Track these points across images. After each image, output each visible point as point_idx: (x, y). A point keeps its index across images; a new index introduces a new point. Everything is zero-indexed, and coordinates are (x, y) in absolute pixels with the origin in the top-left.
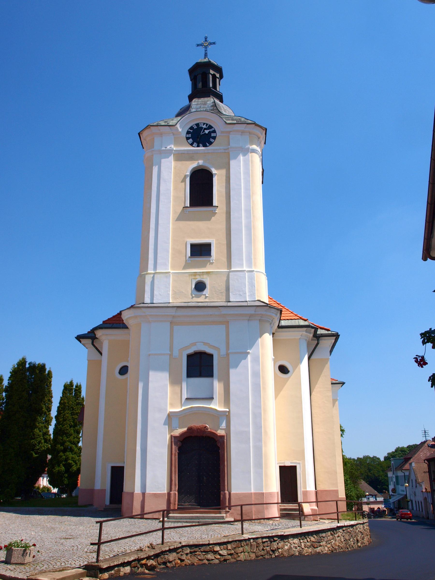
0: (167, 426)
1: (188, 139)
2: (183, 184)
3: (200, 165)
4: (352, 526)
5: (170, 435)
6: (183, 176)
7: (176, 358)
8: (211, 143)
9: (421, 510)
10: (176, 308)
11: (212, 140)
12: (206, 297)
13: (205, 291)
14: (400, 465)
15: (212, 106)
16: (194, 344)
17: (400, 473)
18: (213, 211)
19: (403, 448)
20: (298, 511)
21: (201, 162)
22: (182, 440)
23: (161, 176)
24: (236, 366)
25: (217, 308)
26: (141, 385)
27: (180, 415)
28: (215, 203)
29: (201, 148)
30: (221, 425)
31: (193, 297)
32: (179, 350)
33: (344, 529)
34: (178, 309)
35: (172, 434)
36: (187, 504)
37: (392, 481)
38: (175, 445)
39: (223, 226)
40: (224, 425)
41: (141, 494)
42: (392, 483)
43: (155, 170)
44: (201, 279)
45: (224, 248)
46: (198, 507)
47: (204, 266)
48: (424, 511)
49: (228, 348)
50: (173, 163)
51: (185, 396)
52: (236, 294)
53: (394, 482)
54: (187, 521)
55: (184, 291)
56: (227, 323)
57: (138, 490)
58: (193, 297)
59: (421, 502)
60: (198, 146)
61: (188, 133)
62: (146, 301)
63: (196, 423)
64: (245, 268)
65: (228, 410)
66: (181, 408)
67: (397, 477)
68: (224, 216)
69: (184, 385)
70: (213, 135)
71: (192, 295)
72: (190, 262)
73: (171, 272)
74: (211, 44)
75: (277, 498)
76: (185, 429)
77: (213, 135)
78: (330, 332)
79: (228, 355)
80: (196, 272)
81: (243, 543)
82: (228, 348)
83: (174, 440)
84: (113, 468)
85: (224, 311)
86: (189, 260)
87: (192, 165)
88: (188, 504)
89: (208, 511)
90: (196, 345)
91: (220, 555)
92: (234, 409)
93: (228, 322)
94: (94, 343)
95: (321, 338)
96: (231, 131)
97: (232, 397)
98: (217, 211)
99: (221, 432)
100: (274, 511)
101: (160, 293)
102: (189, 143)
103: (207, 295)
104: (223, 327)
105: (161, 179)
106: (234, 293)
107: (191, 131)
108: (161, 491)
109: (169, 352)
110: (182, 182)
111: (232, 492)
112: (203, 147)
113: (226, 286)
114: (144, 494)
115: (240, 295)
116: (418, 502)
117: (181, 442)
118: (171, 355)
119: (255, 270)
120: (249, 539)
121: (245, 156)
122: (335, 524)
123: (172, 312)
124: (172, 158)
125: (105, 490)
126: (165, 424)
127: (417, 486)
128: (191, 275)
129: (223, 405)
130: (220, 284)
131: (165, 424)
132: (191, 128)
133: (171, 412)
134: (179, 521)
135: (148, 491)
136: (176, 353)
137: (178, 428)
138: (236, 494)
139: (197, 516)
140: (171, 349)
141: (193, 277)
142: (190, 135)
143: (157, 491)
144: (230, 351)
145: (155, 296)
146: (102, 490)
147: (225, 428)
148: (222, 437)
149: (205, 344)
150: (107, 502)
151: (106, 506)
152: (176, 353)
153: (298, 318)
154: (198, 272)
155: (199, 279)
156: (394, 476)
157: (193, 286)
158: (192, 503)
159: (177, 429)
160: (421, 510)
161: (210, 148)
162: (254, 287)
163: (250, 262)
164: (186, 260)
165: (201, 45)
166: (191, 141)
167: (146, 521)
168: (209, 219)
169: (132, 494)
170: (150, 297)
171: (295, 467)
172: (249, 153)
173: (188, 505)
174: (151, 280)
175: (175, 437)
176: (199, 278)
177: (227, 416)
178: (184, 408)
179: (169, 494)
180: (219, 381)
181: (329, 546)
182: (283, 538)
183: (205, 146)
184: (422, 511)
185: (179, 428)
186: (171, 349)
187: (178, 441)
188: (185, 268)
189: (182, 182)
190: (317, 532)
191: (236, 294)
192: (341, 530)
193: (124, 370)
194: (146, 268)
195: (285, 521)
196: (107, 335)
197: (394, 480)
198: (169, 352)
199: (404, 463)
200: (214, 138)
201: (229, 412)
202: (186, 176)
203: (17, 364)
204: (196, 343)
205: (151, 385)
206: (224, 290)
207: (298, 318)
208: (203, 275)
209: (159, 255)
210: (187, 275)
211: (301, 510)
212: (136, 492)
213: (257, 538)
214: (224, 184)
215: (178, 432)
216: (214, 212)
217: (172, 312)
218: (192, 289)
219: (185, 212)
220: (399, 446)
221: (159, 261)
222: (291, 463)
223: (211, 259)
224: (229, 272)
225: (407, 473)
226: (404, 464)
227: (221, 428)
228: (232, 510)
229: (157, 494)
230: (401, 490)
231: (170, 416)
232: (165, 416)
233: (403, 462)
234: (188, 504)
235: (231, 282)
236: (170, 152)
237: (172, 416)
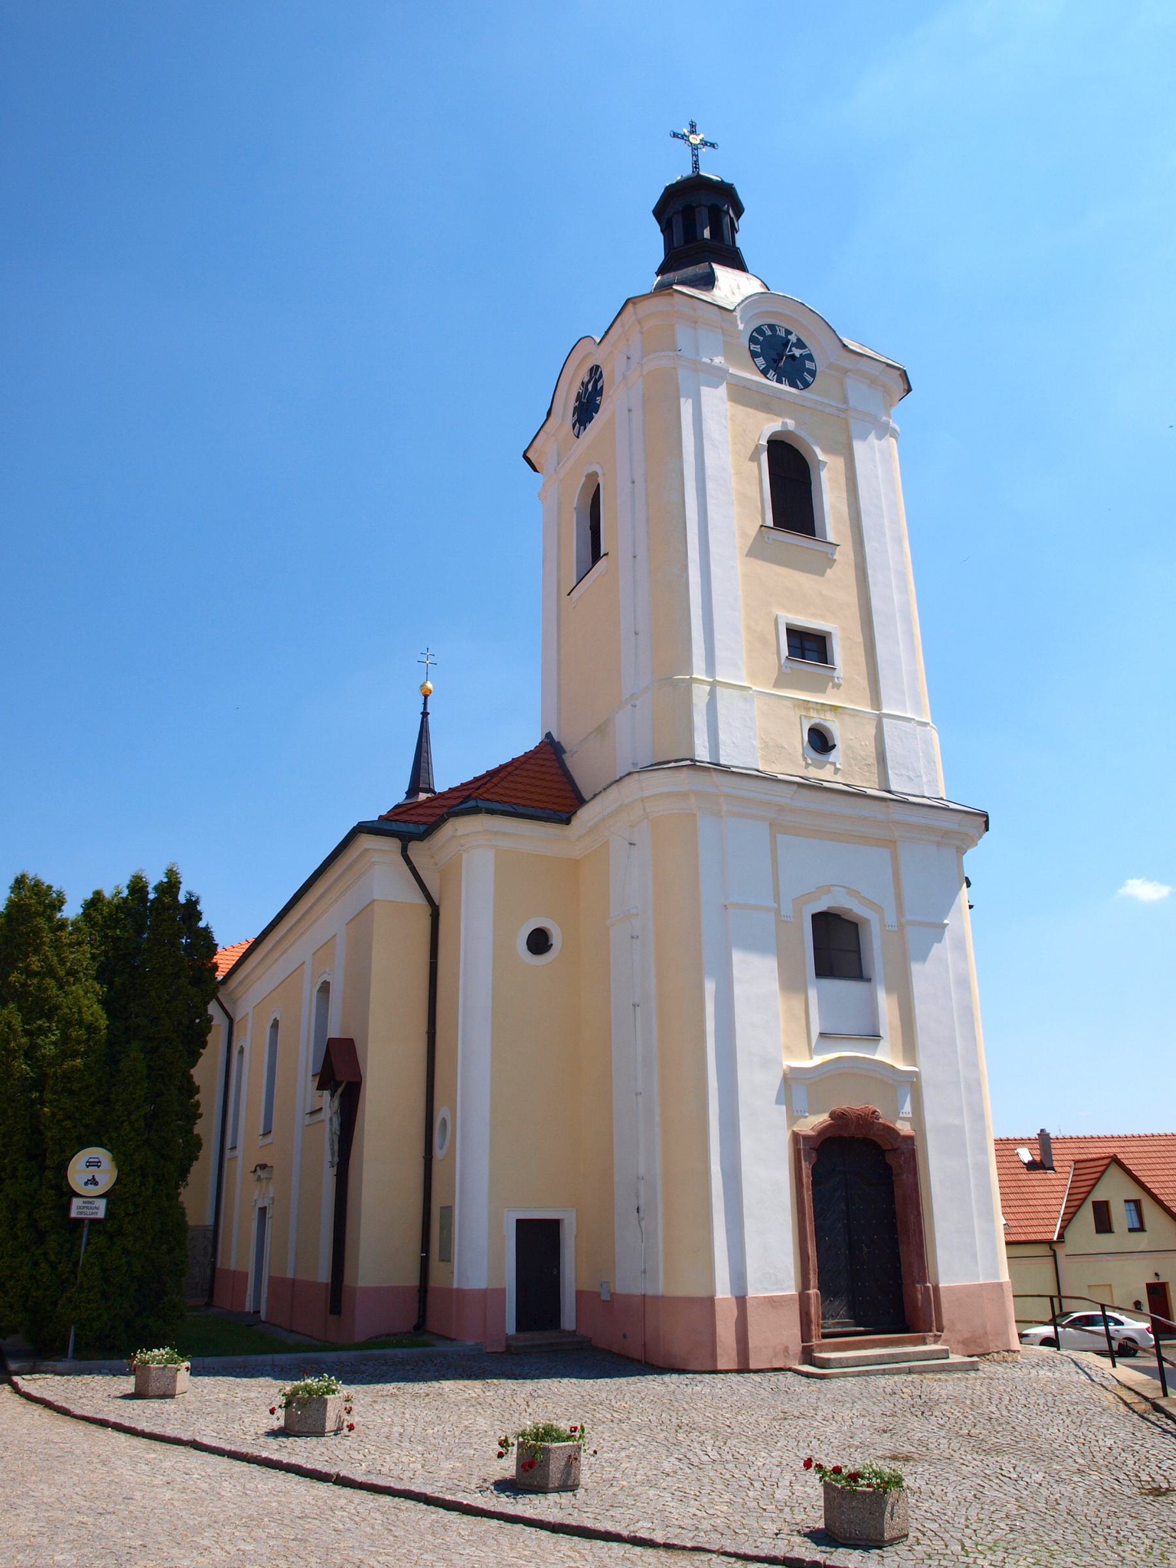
0: (784, 1108)
3: (790, 431)
5: (790, 1132)
7: (787, 922)
12: (837, 770)
13: (834, 752)
16: (827, 889)
18: (827, 553)
21: (791, 424)
22: (817, 1147)
23: (704, 427)
24: (923, 957)
25: (884, 804)
26: (710, 987)
29: (785, 387)
30: (902, 1109)
31: (807, 765)
32: (793, 900)
35: (795, 1129)
36: (831, 1321)
38: (806, 1161)
40: (907, 1109)
41: (734, 1300)
43: (686, 407)
44: (822, 722)
45: (860, 652)
46: (858, 1329)
51: (815, 1030)
52: (901, 775)
54: (884, 1370)
55: (786, 746)
57: (723, 1291)
58: (807, 765)
62: (698, 755)
63: (852, 1103)
66: (811, 1058)
68: (851, 573)
69: (813, 994)
70: (808, 364)
71: (805, 759)
72: (789, 671)
79: (901, 926)
80: (808, 701)
84: (520, 1222)
86: (786, 667)
87: (772, 425)
88: (834, 1321)
89: (899, 1338)
90: (829, 891)
93: (895, 842)
94: (409, 853)
97: (922, 1038)
101: (734, 740)
102: (758, 368)
103: (838, 766)
105: (704, 436)
106: (897, 772)
108: (782, 1290)
111: (940, 1285)
112: (790, 386)
113: (876, 751)
114: (741, 1301)
115: (911, 779)
117: (816, 1150)
118: (778, 912)
121: (880, 440)
123: (783, 796)
124: (723, 390)
125: (504, 1290)
126: (778, 1102)
128: (799, 706)
129: (901, 1054)
130: (863, 743)
131: (778, 1102)
132: (759, 330)
133: (793, 1069)
134: (867, 1371)
135: (751, 1293)
137: (807, 1114)
138: (944, 1287)
139: (892, 1355)
140: (777, 898)
141: (803, 713)
143: (772, 1291)
145: (722, 747)
146: (496, 1290)
147: (910, 1115)
148: (910, 1139)
149: (852, 892)
150: (511, 1328)
151: (508, 1338)
152: (787, 910)
154: (812, 702)
155: (817, 721)
157: (806, 738)
158: (841, 1318)
159: (806, 1117)
161: (805, 393)
162: (932, 764)
164: (780, 666)
165: (683, 139)
166: (761, 361)
167: (756, 1378)
169: (711, 1300)
170: (707, 744)
172: (888, 435)
173: (833, 1323)
174: (707, 698)
175: (806, 1138)
176: (816, 718)
177: (913, 1083)
178: (818, 1060)
179: (803, 1299)
180: (889, 990)
183: (793, 384)
185: (810, 1114)
186: (777, 898)
187: (811, 1149)
188: (777, 685)
191: (901, 775)
193: (539, 942)
194: (687, 665)
196: (496, 833)
203: (128, 887)
204: (832, 888)
205: (737, 989)
206: (872, 760)
208: (825, 711)
209: (718, 636)
210: (787, 703)
212: (719, 1295)
214: (844, 495)
215: (814, 1122)
216: (830, 556)
217: (783, 796)
218: (805, 744)
219: (766, 540)
221: (719, 653)
227: (901, 1115)
228: (945, 1331)
229: (775, 1299)
231: (791, 1080)
234: (834, 1321)
235: (887, 741)
237: (792, 1079)
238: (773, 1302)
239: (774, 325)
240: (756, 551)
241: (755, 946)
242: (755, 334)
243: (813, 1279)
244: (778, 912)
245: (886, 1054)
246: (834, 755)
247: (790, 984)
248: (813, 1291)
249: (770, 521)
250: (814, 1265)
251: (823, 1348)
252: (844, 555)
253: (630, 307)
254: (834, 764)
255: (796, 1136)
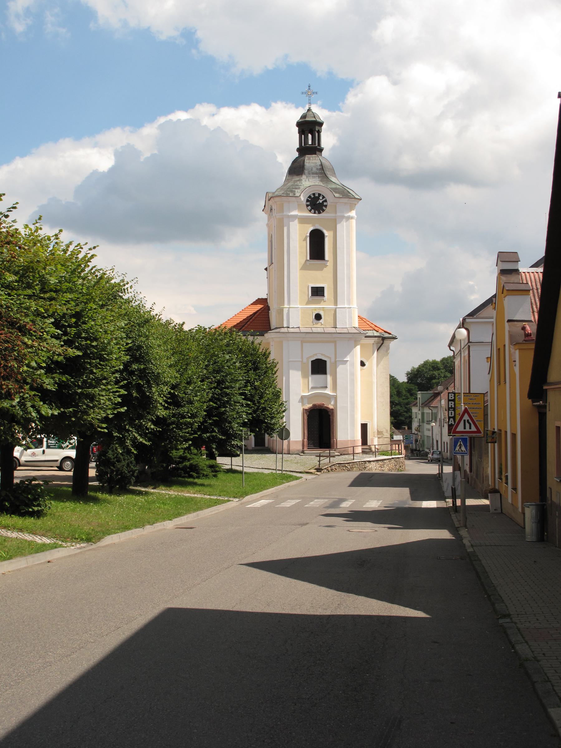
1: (307, 206)
2: (305, 242)
4: (398, 458)
6: (305, 236)
8: (323, 211)
9: (446, 451)
10: (305, 334)
11: (324, 208)
13: (321, 320)
14: (428, 400)
15: (320, 169)
16: (316, 354)
17: (427, 410)
19: (434, 362)
20: (488, 445)
27: (309, 398)
28: (327, 257)
33: (395, 459)
34: (307, 334)
37: (416, 418)
39: (331, 275)
40: (332, 403)
42: (416, 420)
43: (285, 229)
47: (319, 303)
48: (449, 452)
49: (336, 358)
50: (298, 225)
51: (310, 387)
53: (420, 419)
56: (335, 342)
58: (314, 324)
59: (447, 443)
60: (315, 213)
61: (307, 201)
63: (318, 402)
64: (346, 306)
65: (335, 394)
66: (309, 392)
67: (423, 414)
70: (325, 204)
73: (300, 307)
74: (314, 93)
75: (360, 443)
76: (311, 405)
77: (325, 204)
78: (391, 336)
81: (355, 463)
82: (336, 358)
83: (305, 411)
85: (334, 335)
91: (347, 468)
92: (339, 394)
95: (385, 340)
96: (338, 202)
98: (328, 264)
99: (331, 407)
100: (359, 450)
103: (322, 323)
104: (332, 345)
107: (310, 199)
109: (301, 360)
110: (304, 240)
116: (444, 442)
118: (302, 361)
119: (352, 307)
120: (357, 462)
122: (390, 457)
124: (296, 221)
127: (503, 346)
132: (310, 197)
136: (305, 360)
142: (308, 203)
144: (337, 360)
148: (332, 409)
149: (322, 354)
152: (305, 360)
153: (373, 329)
156: (420, 412)
157: (314, 317)
160: (446, 451)
163: (349, 302)
164: (308, 299)
166: (309, 208)
168: (322, 270)
171: (367, 424)
175: (306, 410)
177: (335, 398)
178: (310, 393)
179: (303, 441)
180: (330, 375)
181: (388, 467)
182: (369, 462)
184: (447, 452)
189: (304, 240)
190: (383, 460)
192: (393, 460)
195: (365, 455)
197: (420, 416)
198: (301, 360)
199: (433, 397)
200: (326, 206)
201: (336, 396)
202: (306, 236)
203: (170, 120)
207: (373, 329)
211: (370, 449)
213: (360, 462)
215: (308, 406)
220: (429, 359)
222: (365, 422)
223: (324, 298)
224: (336, 308)
225: (435, 411)
226: (433, 399)
230: (427, 429)
231: (303, 398)
232: (300, 397)
233: (432, 396)
236: (295, 217)
238: (296, 442)
239: (314, 193)
240: (304, 267)
241: (296, 369)
242: (308, 199)
243: (306, 437)
244: (302, 361)
245: (328, 391)
246: (322, 321)
247: (305, 376)
248: (306, 440)
249: (308, 258)
250: (189, 492)
251: (306, 451)
252: (330, 264)
253: (272, 199)
254: (321, 323)
255: (304, 409)
